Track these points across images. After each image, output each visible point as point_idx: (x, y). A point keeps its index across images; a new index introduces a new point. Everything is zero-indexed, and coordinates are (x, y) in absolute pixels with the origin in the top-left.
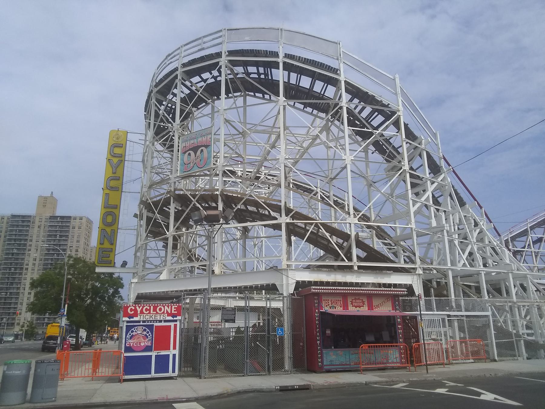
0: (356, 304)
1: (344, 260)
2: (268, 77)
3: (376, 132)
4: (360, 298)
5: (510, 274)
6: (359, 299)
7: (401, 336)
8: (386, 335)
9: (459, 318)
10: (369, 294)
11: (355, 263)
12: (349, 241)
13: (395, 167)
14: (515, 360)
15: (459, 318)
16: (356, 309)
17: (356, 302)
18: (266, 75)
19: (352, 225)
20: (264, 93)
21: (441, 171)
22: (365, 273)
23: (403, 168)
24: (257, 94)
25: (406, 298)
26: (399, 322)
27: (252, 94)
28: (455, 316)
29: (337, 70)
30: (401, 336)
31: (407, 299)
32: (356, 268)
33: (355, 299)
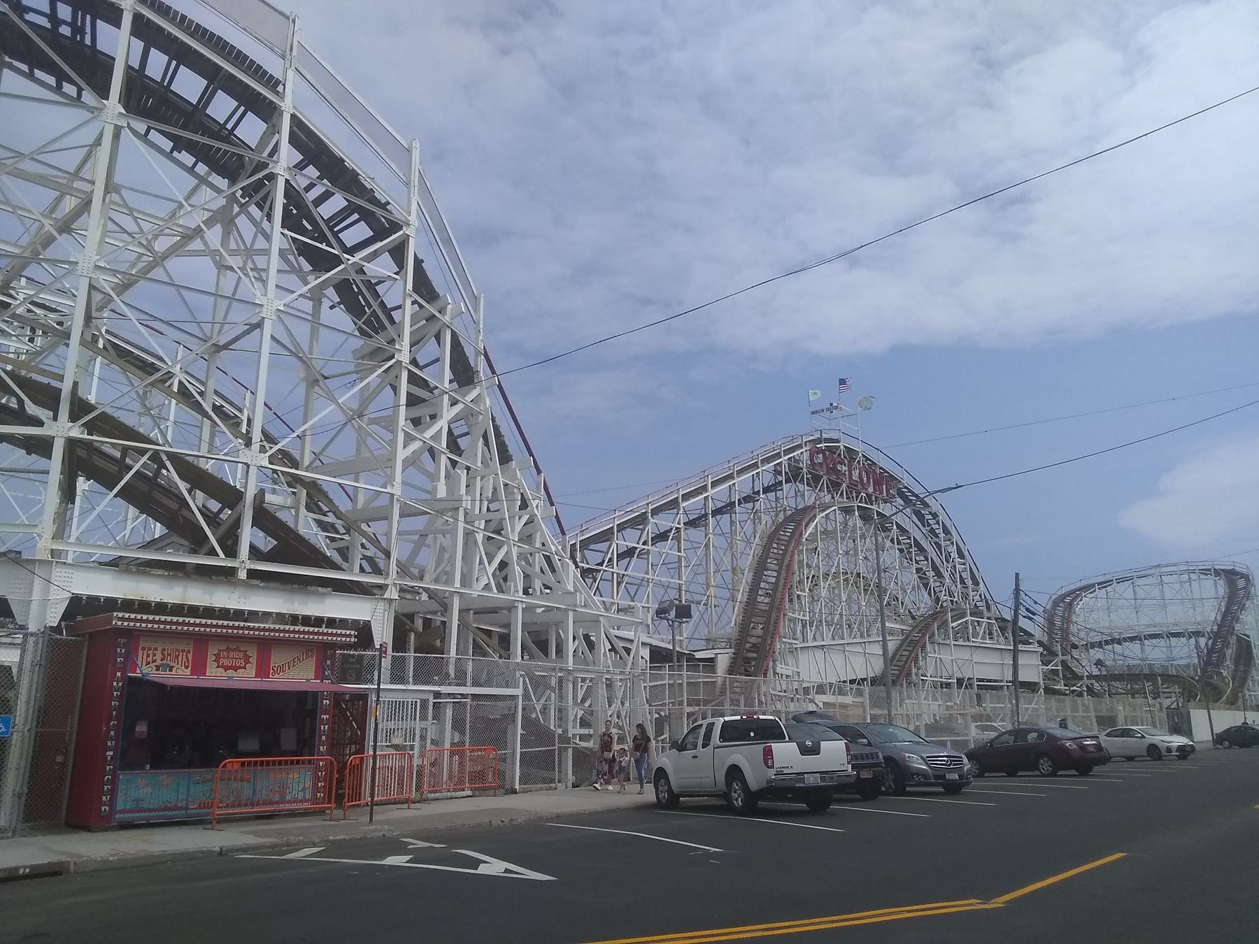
0: (226, 662)
2: (83, 38)
3: (349, 260)
5: (571, 614)
6: (237, 650)
7: (324, 738)
10: (264, 639)
11: (243, 562)
12: (238, 508)
14: (551, 789)
17: (228, 657)
18: (78, 30)
19: (253, 470)
20: (61, 77)
22: (263, 588)
24: (38, 74)
27: (25, 68)
29: (278, 82)
30: (324, 738)
32: (242, 575)
33: (228, 650)
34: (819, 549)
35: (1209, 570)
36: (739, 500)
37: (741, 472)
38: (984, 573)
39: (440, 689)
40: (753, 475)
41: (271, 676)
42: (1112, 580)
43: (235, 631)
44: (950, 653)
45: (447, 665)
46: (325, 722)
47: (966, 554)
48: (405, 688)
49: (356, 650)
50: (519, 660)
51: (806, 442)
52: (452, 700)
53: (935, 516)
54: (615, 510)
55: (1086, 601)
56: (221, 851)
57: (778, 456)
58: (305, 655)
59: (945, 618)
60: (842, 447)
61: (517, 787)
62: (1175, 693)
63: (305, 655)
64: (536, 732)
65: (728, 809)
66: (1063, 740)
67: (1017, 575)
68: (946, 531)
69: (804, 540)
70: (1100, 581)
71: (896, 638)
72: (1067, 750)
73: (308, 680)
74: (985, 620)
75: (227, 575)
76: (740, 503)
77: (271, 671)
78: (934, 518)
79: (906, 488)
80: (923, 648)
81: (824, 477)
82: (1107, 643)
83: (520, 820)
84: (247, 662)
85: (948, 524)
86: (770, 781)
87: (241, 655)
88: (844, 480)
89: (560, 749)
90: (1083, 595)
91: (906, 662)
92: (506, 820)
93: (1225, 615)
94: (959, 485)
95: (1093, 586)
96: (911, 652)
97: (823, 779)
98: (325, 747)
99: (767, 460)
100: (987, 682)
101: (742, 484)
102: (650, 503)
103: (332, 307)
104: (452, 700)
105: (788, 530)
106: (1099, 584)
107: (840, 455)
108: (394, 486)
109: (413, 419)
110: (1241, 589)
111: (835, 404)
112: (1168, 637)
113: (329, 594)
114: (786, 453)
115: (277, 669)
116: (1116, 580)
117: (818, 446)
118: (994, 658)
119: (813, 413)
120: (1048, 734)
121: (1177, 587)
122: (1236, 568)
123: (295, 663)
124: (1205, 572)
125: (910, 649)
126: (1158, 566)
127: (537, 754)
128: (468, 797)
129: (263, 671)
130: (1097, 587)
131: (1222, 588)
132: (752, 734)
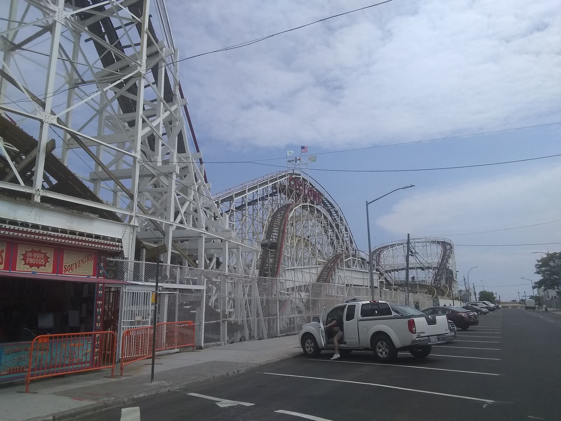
0: (31, 261)
1: (18, 183)
4: (43, 251)
5: (227, 243)
6: (39, 252)
7: (99, 317)
8: (74, 317)
9: (172, 292)
12: (33, 154)
13: (112, 74)
14: (218, 345)
15: (172, 292)
16: (30, 270)
17: (33, 257)
19: (46, 126)
21: (174, 100)
22: (52, 210)
23: (138, 69)
25: (111, 259)
26: (99, 296)
28: (167, 289)
30: (99, 317)
31: (112, 261)
32: (37, 199)
33: (33, 252)
34: (294, 223)
35: (435, 241)
36: (259, 198)
37: (260, 185)
38: (355, 238)
39: (163, 285)
40: (263, 188)
41: (63, 273)
42: (396, 244)
43: (37, 237)
44: (344, 273)
45: (165, 269)
46: (99, 307)
47: (348, 229)
48: (143, 284)
49: (113, 258)
50: (203, 269)
51: (288, 174)
52: (168, 292)
53: (336, 212)
54: (217, 194)
55: (385, 252)
56: (54, 419)
57: (276, 179)
58: (86, 259)
59: (341, 257)
60: (301, 178)
61: (203, 345)
62: (423, 292)
63: (86, 259)
64: (211, 313)
65: (375, 358)
66: (460, 313)
67: (409, 235)
68: (341, 220)
69: (289, 219)
70: (391, 244)
71: (321, 266)
72: (462, 318)
73: (89, 276)
74: (357, 259)
75: (26, 198)
76: (260, 200)
77: (64, 269)
78: (336, 213)
79: (325, 199)
80: (334, 270)
81: (294, 191)
82: (393, 271)
83: (242, 371)
84: (47, 261)
85: (342, 217)
86: (414, 341)
87: (42, 256)
88: (302, 193)
89: (223, 321)
90: (384, 250)
91: (327, 277)
92: (236, 372)
93: (442, 260)
94: (412, 185)
95: (387, 246)
96: (329, 272)
97: (438, 339)
98: (100, 324)
99: (271, 181)
100: (357, 286)
101: (249, 195)
102: (220, 197)
103: (86, 41)
104: (168, 292)
105: (282, 213)
106: (390, 246)
107: (300, 182)
108: (137, 152)
109: (129, 122)
110: (448, 249)
111: (298, 158)
112: (417, 269)
113: (97, 219)
114: (279, 178)
115: (68, 267)
116: (397, 244)
117: (293, 176)
118: (360, 276)
119: (288, 161)
120: (451, 310)
121: (421, 248)
122: (445, 241)
123: (80, 264)
124: (433, 242)
125: (329, 271)
126: (414, 239)
127: (211, 324)
128: (177, 352)
129: (57, 269)
130: (389, 247)
131: (440, 249)
132: (376, 312)
